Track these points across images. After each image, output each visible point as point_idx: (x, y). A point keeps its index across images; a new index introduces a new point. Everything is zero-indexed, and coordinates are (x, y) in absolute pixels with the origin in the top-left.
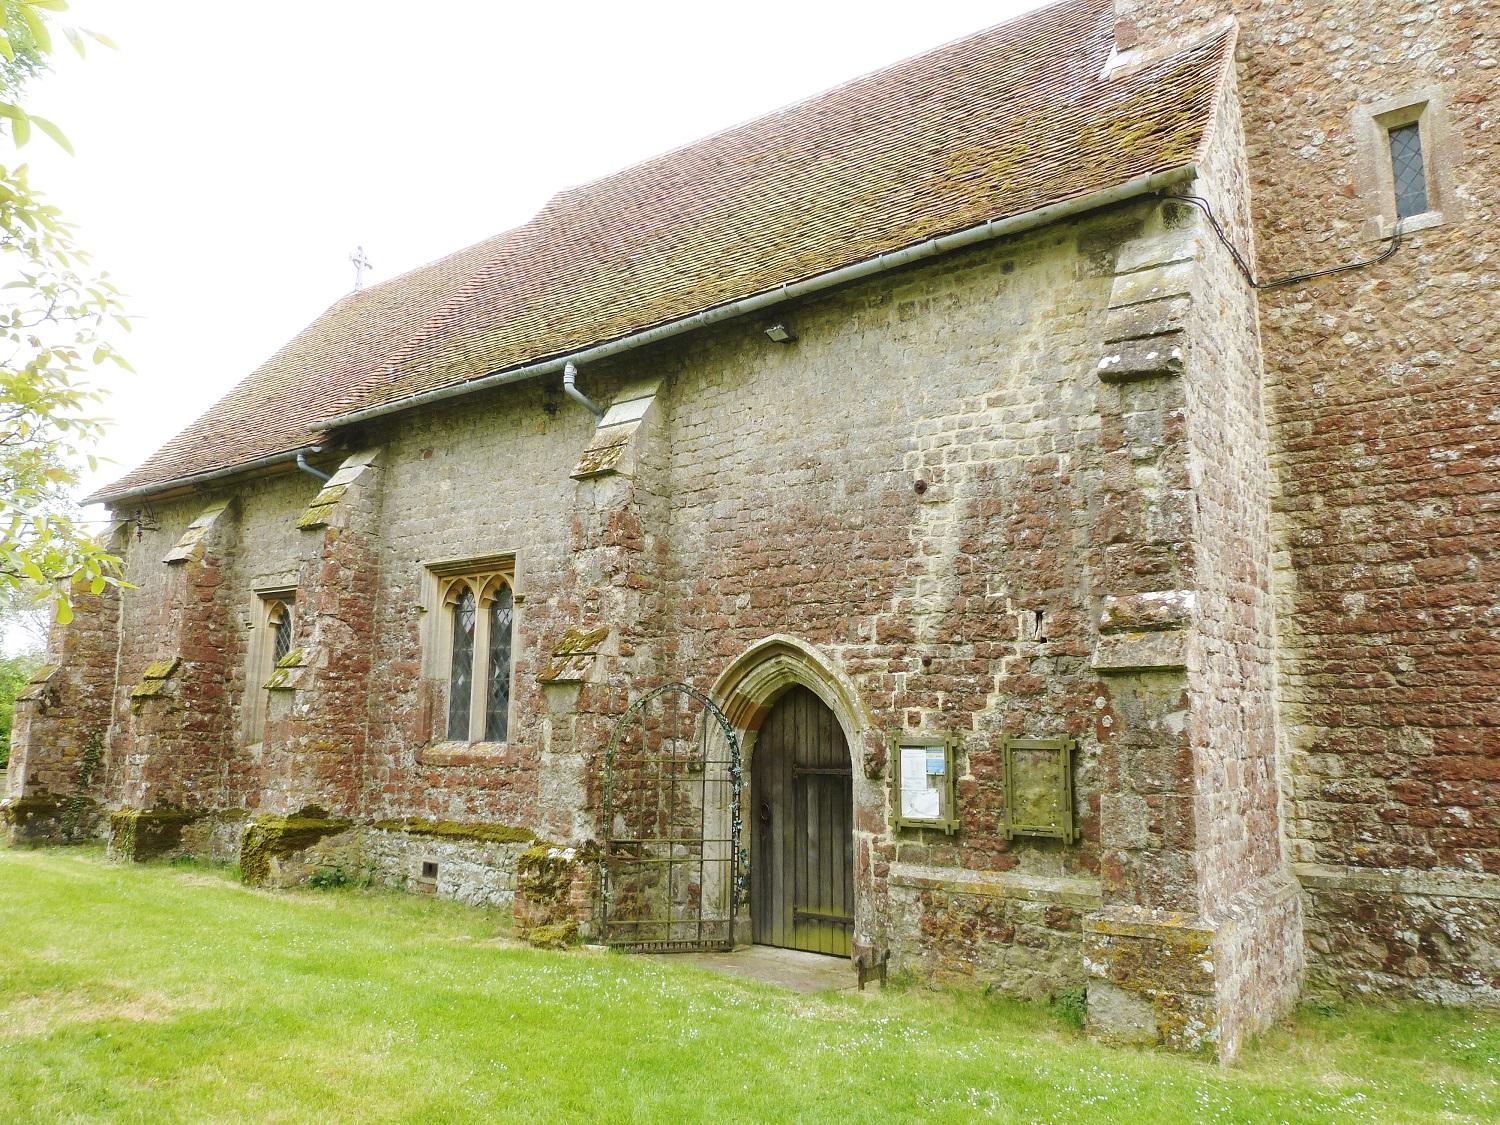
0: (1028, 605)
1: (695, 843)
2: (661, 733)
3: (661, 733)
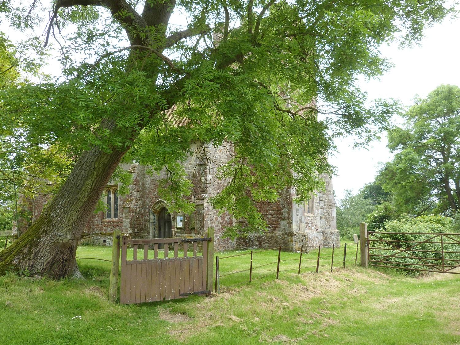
0: (193, 195)
1: (149, 233)
2: (143, 215)
3: (143, 215)
